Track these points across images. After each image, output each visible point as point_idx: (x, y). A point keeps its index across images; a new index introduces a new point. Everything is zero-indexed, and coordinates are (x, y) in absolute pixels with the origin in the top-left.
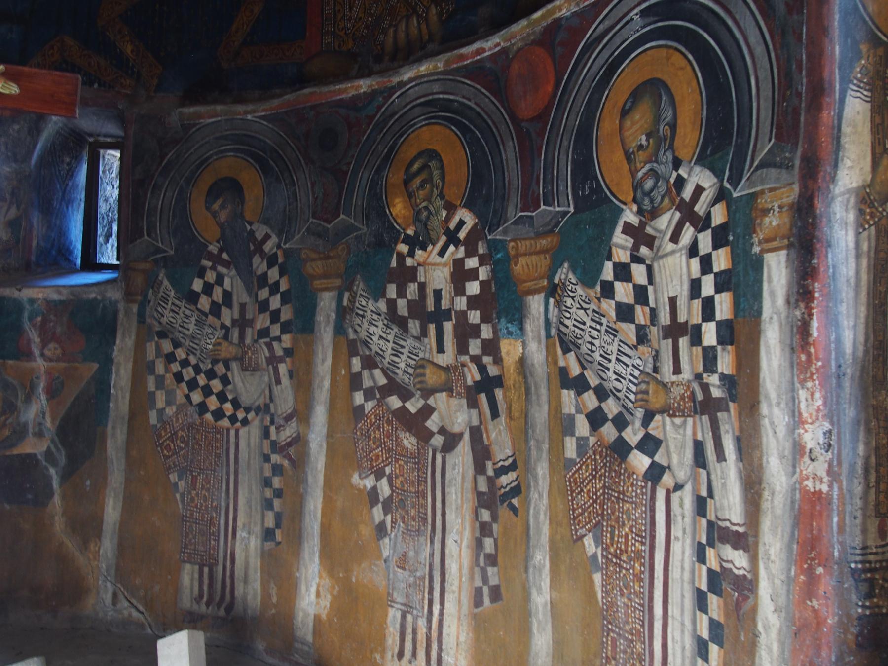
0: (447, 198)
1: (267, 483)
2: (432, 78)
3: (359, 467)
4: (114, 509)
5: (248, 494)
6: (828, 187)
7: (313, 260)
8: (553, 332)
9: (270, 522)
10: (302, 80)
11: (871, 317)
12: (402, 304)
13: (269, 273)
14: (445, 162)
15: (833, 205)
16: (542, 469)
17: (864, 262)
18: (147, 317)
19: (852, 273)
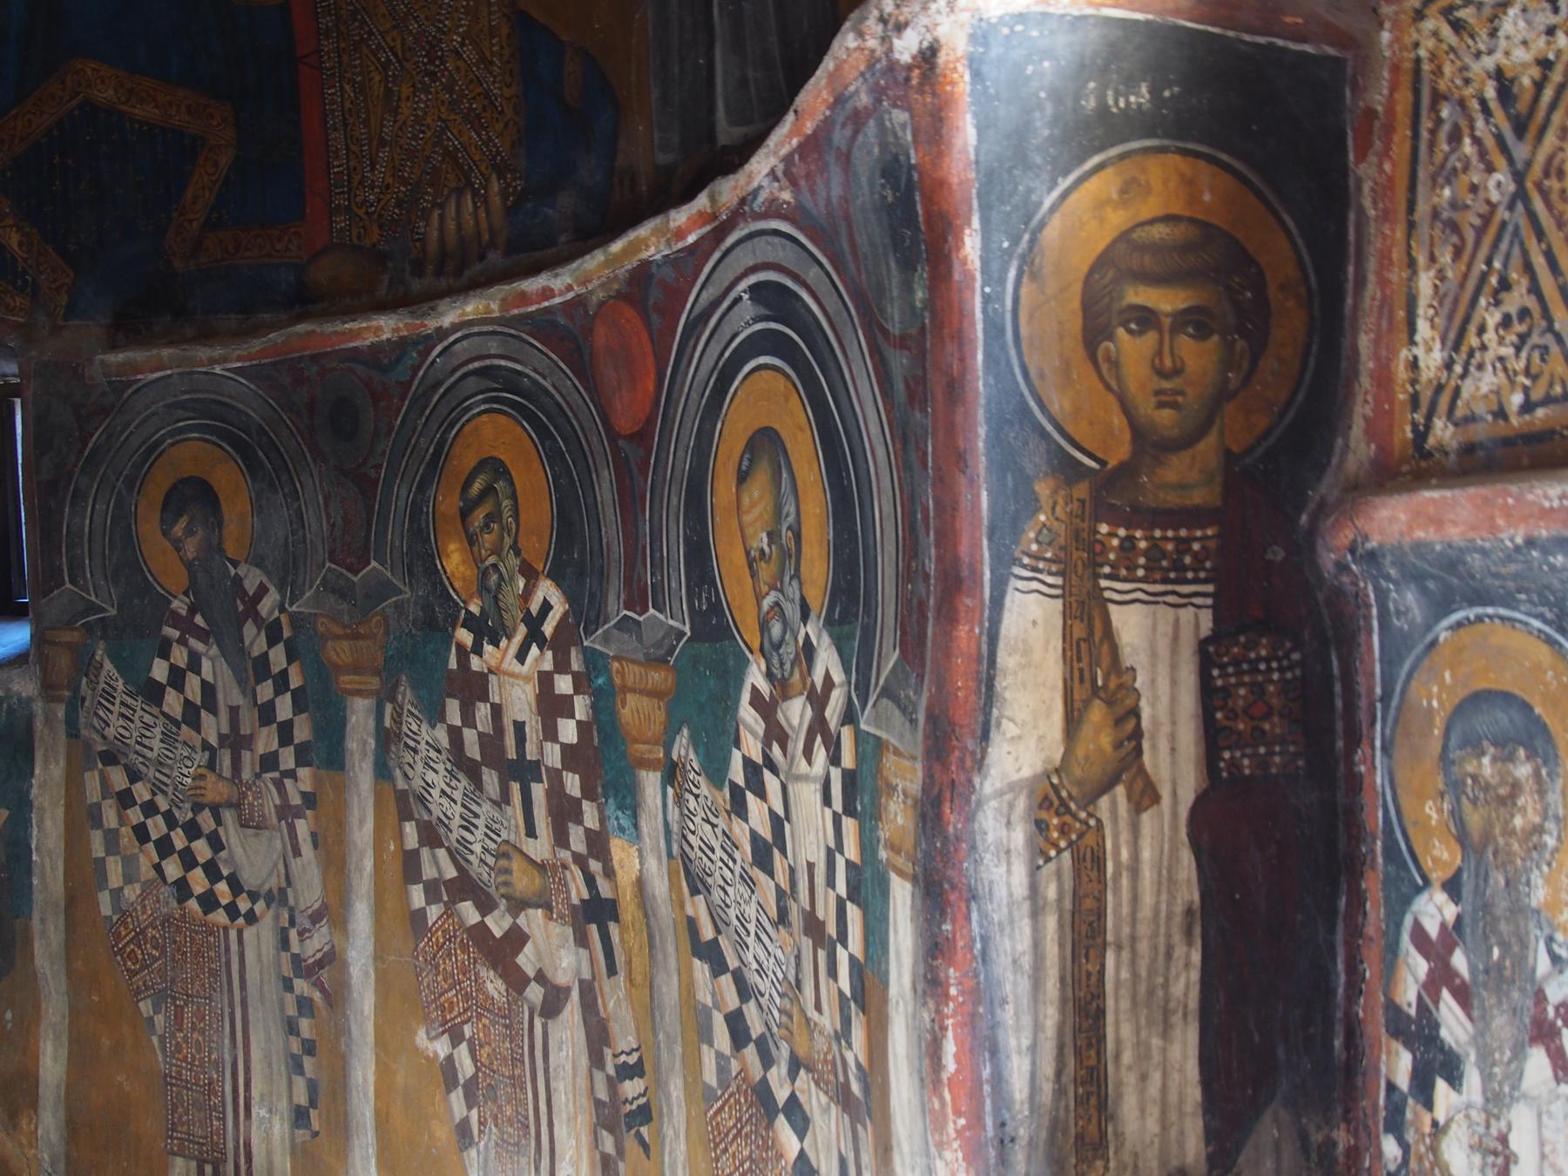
0: (524, 554)
1: (292, 1028)
2: (485, 329)
3: (426, 1018)
4: (55, 1059)
5: (265, 1045)
6: (970, 781)
7: (337, 637)
8: (675, 848)
9: (302, 1098)
10: (306, 300)
11: (1069, 1023)
12: (470, 736)
13: (272, 654)
14: (518, 486)
15: (980, 816)
16: (676, 1088)
17: (1051, 923)
18: (82, 727)
19: (1023, 942)
